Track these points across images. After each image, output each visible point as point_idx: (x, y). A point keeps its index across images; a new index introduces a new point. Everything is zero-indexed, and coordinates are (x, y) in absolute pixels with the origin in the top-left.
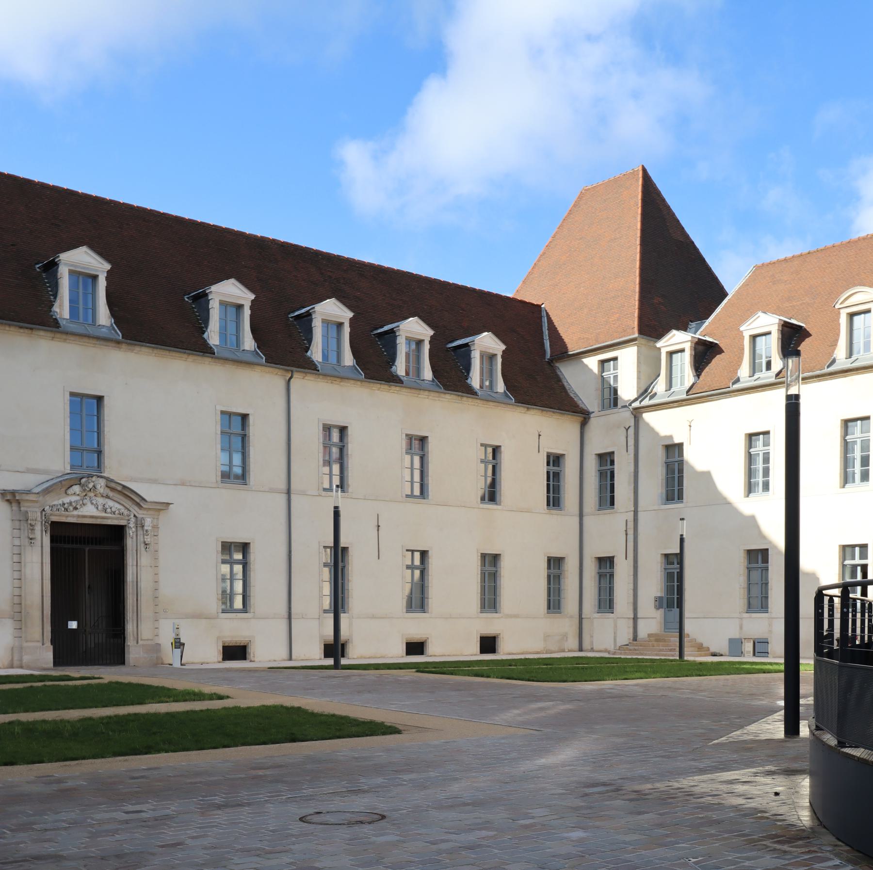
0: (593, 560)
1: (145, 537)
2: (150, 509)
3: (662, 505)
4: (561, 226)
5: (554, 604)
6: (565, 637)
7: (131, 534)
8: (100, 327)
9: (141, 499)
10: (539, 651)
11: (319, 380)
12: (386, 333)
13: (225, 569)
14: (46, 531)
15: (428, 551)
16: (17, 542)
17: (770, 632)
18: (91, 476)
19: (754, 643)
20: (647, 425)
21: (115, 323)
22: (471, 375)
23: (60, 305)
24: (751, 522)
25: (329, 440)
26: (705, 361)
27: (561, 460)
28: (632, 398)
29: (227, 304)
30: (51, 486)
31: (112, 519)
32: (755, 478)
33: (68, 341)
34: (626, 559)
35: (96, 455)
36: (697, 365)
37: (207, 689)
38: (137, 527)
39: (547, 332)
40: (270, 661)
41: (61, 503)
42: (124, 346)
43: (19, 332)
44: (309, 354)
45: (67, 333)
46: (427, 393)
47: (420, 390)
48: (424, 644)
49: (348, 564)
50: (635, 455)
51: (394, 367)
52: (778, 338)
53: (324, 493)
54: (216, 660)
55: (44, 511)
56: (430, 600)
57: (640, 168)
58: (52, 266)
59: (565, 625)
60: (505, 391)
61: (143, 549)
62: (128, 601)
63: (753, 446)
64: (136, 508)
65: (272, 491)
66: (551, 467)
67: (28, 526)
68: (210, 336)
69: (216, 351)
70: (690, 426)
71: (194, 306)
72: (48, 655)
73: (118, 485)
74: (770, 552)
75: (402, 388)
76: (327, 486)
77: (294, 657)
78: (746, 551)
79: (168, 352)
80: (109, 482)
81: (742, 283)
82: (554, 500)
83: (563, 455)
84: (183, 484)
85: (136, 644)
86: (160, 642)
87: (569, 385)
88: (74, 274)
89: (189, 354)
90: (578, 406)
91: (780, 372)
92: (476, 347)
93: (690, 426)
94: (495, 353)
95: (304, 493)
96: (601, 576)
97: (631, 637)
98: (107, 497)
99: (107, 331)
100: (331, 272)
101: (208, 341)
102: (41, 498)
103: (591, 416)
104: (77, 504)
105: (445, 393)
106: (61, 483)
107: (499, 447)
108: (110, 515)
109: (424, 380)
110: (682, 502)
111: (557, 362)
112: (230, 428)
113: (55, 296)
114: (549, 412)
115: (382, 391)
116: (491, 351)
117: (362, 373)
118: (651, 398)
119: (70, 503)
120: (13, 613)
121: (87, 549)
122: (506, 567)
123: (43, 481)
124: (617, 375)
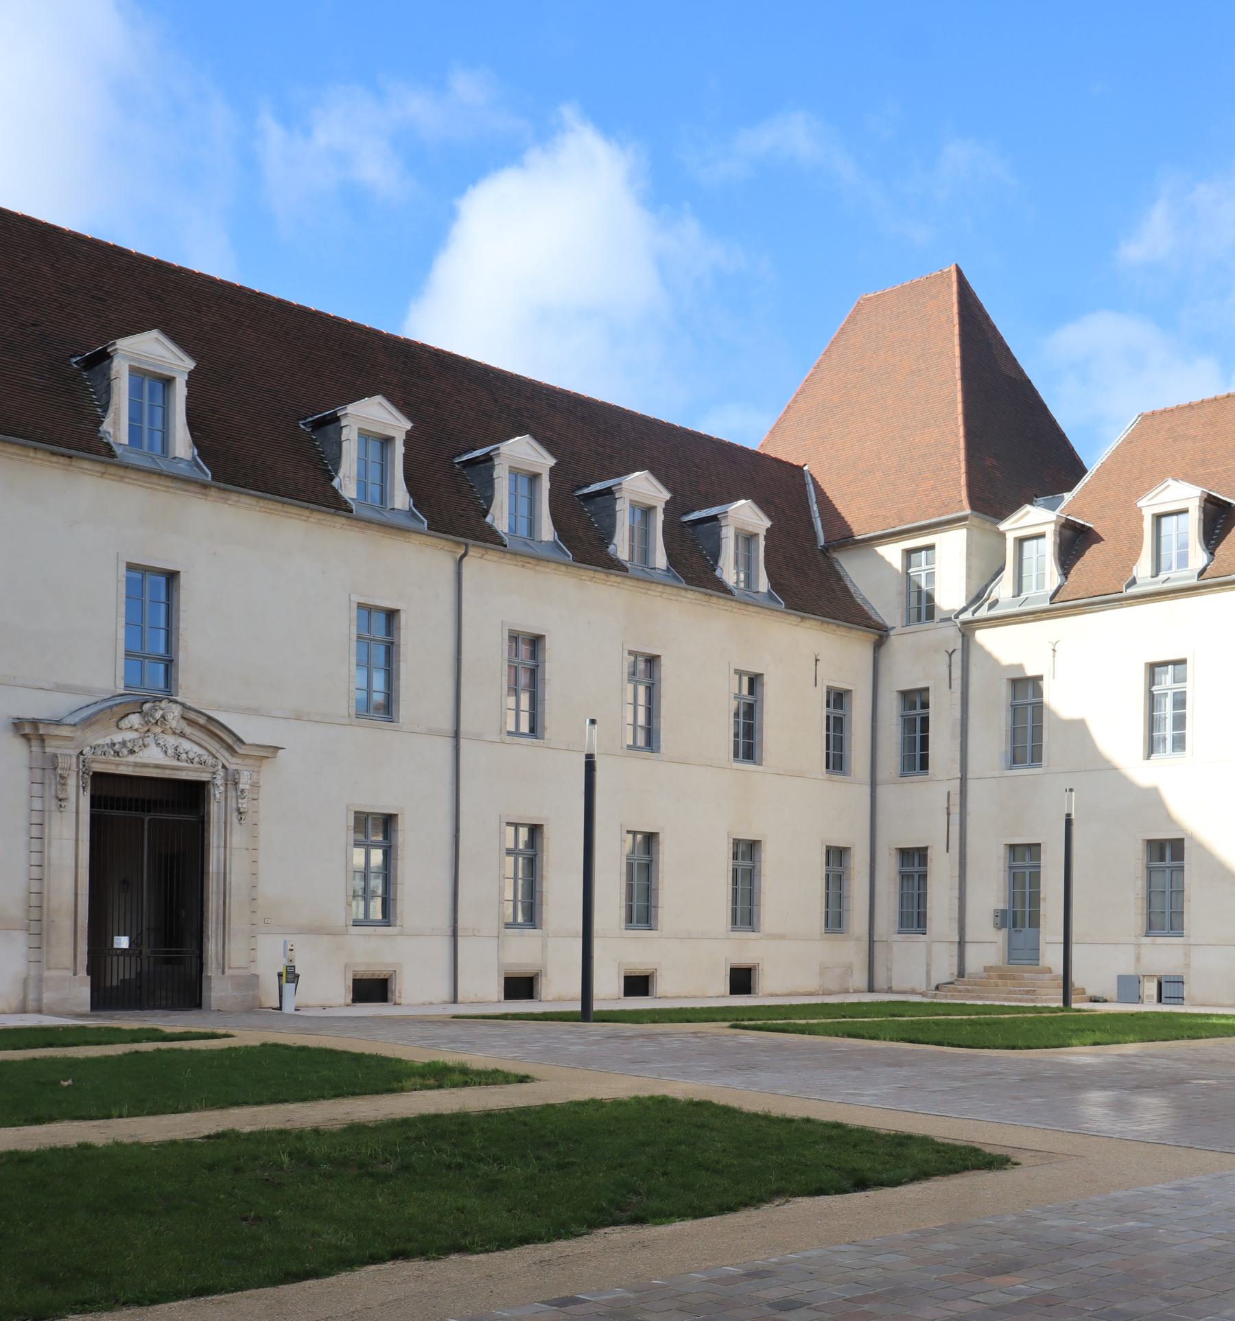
0: (894, 852)
1: (240, 801)
2: (248, 756)
3: (1006, 769)
4: (828, 350)
5: (835, 920)
6: (848, 970)
7: (218, 796)
8: (175, 461)
9: (235, 739)
10: (813, 991)
11: (504, 561)
12: (599, 493)
13: (358, 856)
14: (84, 788)
15: (657, 833)
16: (37, 804)
17: (1187, 966)
18: (158, 700)
19: (1160, 985)
20: (981, 647)
21: (198, 455)
22: (720, 563)
23: (114, 423)
24: (1152, 798)
25: (516, 656)
26: (1074, 552)
27: (845, 700)
28: (959, 607)
29: (368, 436)
30: (95, 714)
31: (187, 770)
32: (1159, 731)
33: (126, 480)
34: (948, 851)
35: (162, 667)
36: (1062, 558)
37: (477, 1060)
38: (226, 784)
39: (815, 507)
40: (424, 1004)
41: (109, 742)
42: (213, 493)
43: (51, 462)
44: (488, 519)
45: (126, 467)
46: (660, 588)
47: (652, 582)
48: (650, 978)
49: (543, 851)
50: (962, 693)
51: (611, 547)
52: (1199, 519)
53: (508, 739)
54: (342, 1002)
55: (83, 755)
56: (660, 911)
57: (953, 269)
58: (104, 357)
59: (850, 951)
60: (769, 591)
61: (235, 820)
62: (210, 904)
63: (1156, 682)
64: (227, 754)
65: (431, 732)
66: (832, 709)
67: (56, 779)
68: (343, 484)
69: (354, 508)
70: (1054, 650)
71: (314, 437)
72: (82, 992)
73: (200, 715)
74: (1186, 845)
75: (625, 579)
76: (512, 728)
77: (460, 998)
78: (1146, 842)
79: (280, 505)
80: (186, 710)
81: (1122, 439)
82: (836, 761)
83: (849, 692)
84: (298, 718)
85: (220, 974)
86: (257, 973)
87: (854, 585)
88: (138, 374)
89: (312, 510)
90: (871, 618)
91: (1204, 570)
92: (730, 520)
93: (1054, 650)
94: (757, 532)
95: (478, 738)
96: (905, 877)
97: (955, 970)
98: (182, 735)
99: (187, 467)
100: (509, 398)
101: (340, 491)
102: (79, 734)
103: (891, 634)
104: (134, 745)
105: (686, 590)
106: (111, 711)
107: (760, 676)
108: (185, 764)
109: (655, 569)
110: (1040, 766)
111: (835, 551)
112: (369, 631)
113: (106, 408)
114: (830, 626)
115: (595, 582)
116: (750, 529)
117: (570, 554)
118: (991, 606)
119: (124, 744)
120: (27, 921)
121: (146, 820)
122: (769, 860)
123: (82, 705)
124: (934, 572)
